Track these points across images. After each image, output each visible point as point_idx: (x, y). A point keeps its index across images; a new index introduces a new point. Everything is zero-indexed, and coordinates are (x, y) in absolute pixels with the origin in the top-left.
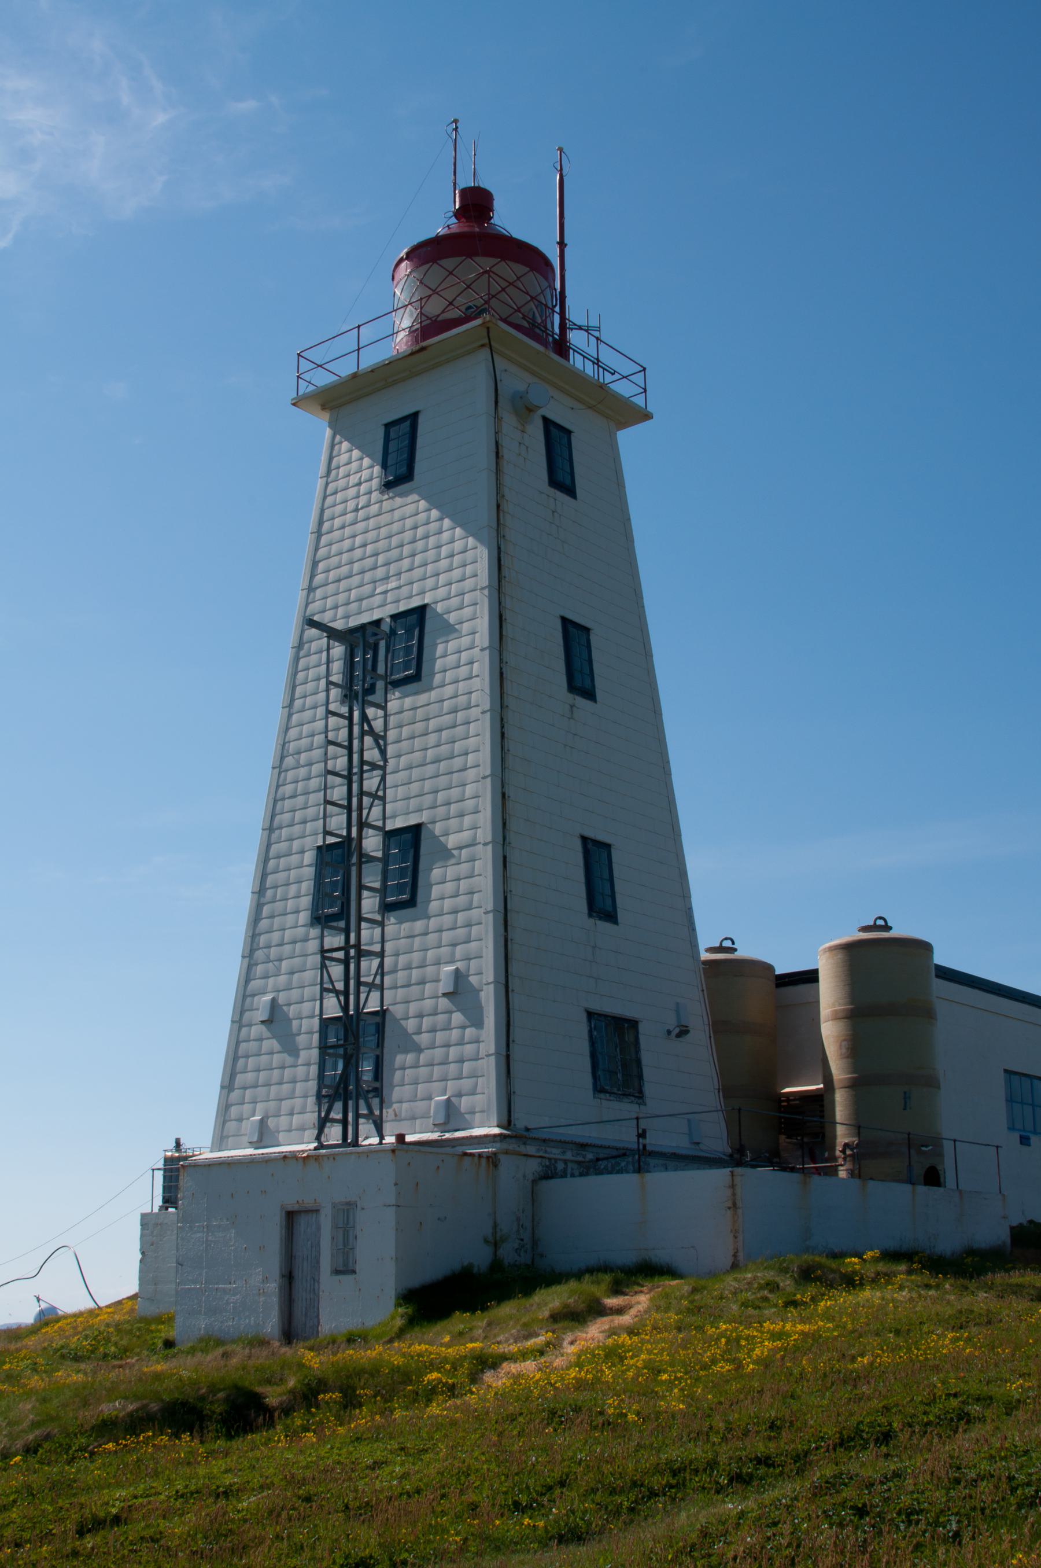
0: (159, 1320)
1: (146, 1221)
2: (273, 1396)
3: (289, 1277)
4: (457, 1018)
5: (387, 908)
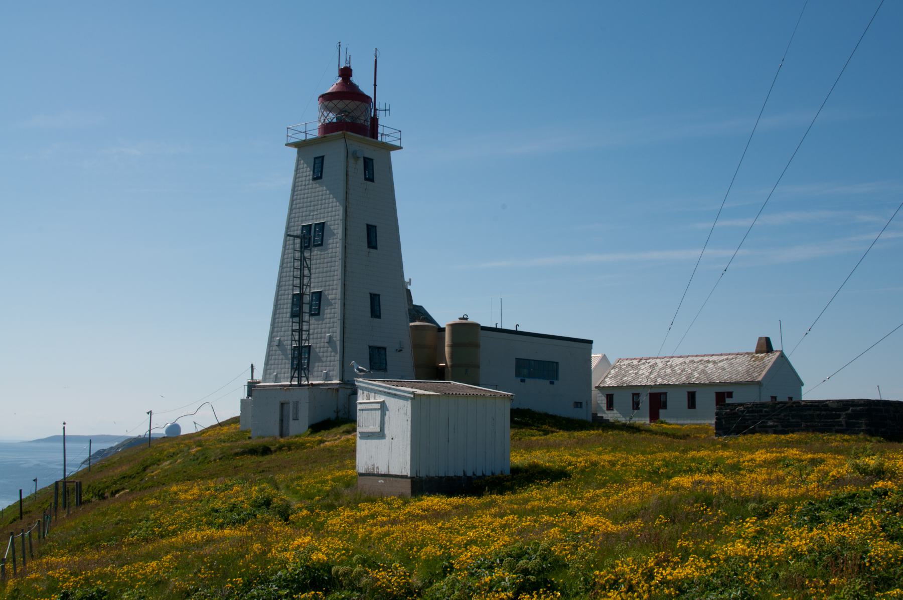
0: (246, 431)
1: (242, 401)
2: (273, 448)
3: (282, 421)
4: (330, 349)
5: (311, 315)
